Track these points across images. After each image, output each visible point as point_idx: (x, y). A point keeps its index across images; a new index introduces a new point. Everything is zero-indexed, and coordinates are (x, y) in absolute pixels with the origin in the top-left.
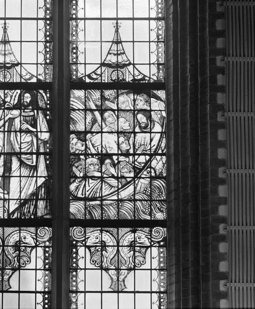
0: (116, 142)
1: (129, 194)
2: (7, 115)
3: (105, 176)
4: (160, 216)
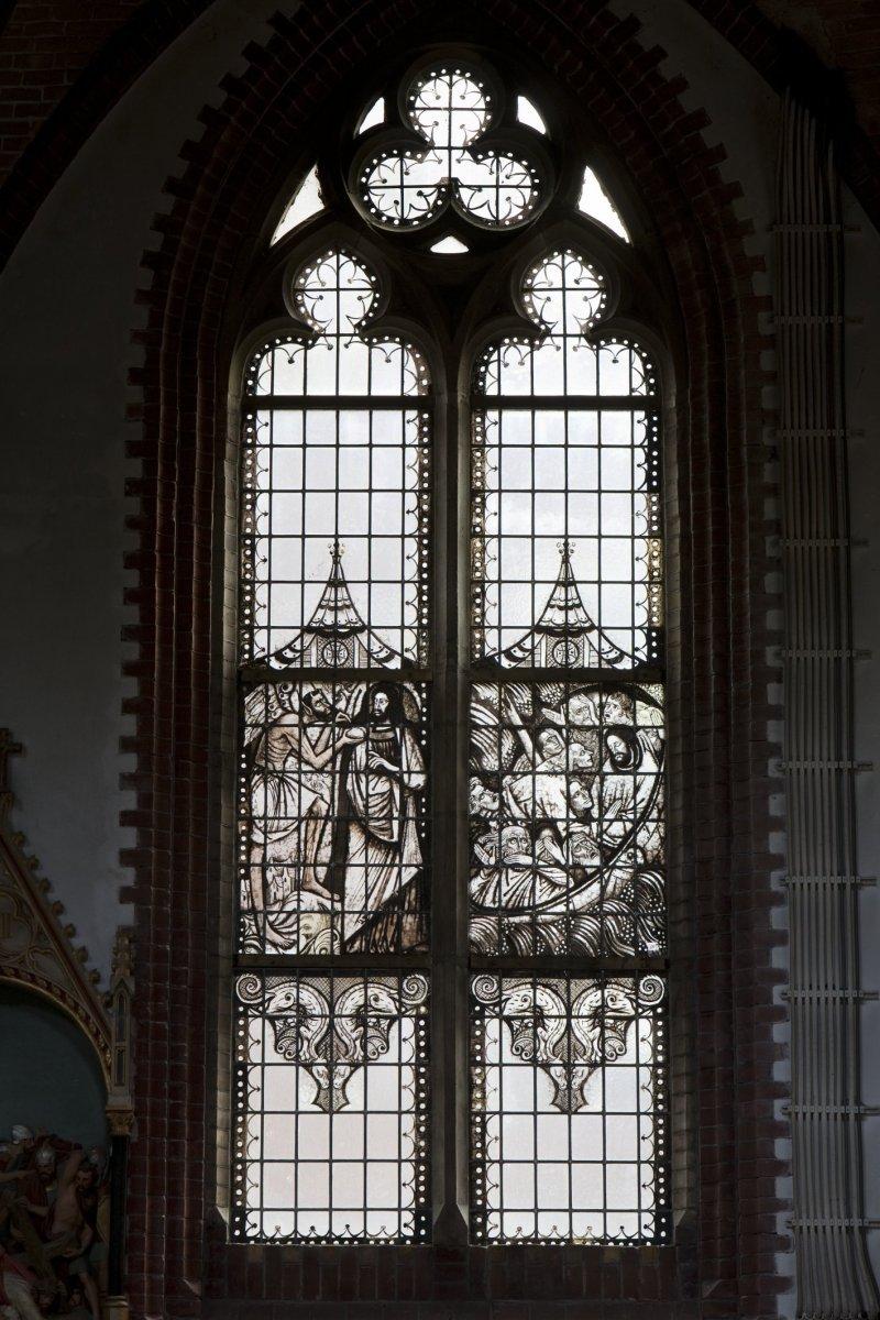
0: (563, 793)
1: (589, 900)
2: (339, 739)
3: (541, 863)
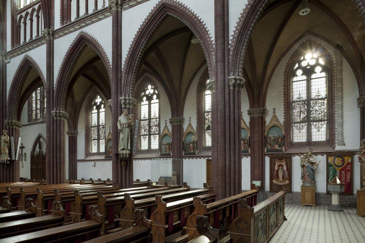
4: (326, 119)
